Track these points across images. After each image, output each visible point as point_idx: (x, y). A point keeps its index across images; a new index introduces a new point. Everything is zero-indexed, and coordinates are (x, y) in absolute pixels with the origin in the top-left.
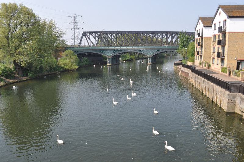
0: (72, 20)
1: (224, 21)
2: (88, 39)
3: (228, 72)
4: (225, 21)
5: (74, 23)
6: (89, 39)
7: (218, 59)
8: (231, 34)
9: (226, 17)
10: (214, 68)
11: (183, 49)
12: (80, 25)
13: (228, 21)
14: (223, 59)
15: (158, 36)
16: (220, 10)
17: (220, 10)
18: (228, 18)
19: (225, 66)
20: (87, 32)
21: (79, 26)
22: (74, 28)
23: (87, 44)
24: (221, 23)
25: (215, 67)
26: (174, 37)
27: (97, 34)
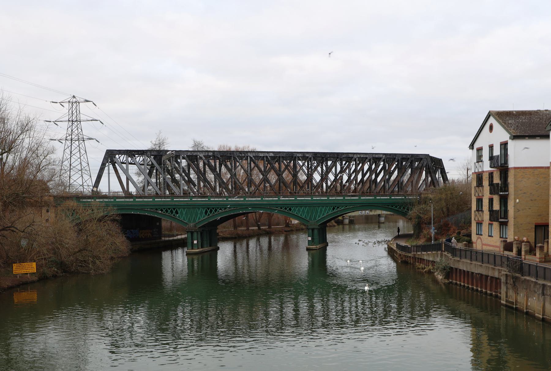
0: (63, 112)
1: (501, 145)
2: (120, 171)
3: (515, 250)
4: (504, 145)
5: (70, 123)
6: (126, 172)
7: (492, 224)
8: (518, 170)
9: (509, 136)
10: (483, 244)
11: (47, 218)
12: (87, 129)
13: (513, 146)
14: (504, 225)
15: (283, 167)
16: (492, 120)
17: (492, 120)
18: (512, 139)
19: (510, 237)
20: (120, 152)
21: (86, 133)
22: (69, 138)
23: (116, 188)
24: (330, 53)
25: (483, 243)
26: (329, 170)
27: (280, 167)
